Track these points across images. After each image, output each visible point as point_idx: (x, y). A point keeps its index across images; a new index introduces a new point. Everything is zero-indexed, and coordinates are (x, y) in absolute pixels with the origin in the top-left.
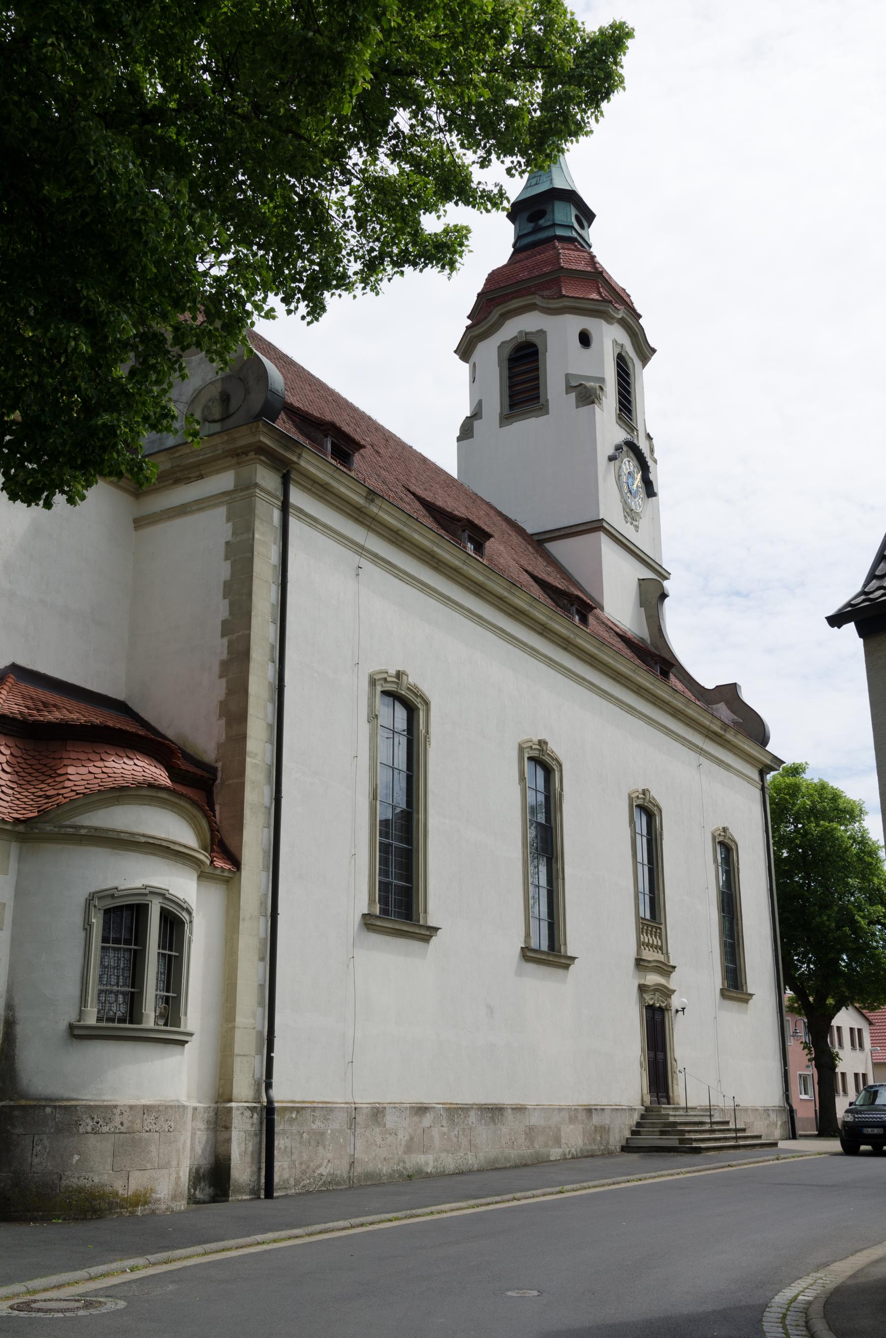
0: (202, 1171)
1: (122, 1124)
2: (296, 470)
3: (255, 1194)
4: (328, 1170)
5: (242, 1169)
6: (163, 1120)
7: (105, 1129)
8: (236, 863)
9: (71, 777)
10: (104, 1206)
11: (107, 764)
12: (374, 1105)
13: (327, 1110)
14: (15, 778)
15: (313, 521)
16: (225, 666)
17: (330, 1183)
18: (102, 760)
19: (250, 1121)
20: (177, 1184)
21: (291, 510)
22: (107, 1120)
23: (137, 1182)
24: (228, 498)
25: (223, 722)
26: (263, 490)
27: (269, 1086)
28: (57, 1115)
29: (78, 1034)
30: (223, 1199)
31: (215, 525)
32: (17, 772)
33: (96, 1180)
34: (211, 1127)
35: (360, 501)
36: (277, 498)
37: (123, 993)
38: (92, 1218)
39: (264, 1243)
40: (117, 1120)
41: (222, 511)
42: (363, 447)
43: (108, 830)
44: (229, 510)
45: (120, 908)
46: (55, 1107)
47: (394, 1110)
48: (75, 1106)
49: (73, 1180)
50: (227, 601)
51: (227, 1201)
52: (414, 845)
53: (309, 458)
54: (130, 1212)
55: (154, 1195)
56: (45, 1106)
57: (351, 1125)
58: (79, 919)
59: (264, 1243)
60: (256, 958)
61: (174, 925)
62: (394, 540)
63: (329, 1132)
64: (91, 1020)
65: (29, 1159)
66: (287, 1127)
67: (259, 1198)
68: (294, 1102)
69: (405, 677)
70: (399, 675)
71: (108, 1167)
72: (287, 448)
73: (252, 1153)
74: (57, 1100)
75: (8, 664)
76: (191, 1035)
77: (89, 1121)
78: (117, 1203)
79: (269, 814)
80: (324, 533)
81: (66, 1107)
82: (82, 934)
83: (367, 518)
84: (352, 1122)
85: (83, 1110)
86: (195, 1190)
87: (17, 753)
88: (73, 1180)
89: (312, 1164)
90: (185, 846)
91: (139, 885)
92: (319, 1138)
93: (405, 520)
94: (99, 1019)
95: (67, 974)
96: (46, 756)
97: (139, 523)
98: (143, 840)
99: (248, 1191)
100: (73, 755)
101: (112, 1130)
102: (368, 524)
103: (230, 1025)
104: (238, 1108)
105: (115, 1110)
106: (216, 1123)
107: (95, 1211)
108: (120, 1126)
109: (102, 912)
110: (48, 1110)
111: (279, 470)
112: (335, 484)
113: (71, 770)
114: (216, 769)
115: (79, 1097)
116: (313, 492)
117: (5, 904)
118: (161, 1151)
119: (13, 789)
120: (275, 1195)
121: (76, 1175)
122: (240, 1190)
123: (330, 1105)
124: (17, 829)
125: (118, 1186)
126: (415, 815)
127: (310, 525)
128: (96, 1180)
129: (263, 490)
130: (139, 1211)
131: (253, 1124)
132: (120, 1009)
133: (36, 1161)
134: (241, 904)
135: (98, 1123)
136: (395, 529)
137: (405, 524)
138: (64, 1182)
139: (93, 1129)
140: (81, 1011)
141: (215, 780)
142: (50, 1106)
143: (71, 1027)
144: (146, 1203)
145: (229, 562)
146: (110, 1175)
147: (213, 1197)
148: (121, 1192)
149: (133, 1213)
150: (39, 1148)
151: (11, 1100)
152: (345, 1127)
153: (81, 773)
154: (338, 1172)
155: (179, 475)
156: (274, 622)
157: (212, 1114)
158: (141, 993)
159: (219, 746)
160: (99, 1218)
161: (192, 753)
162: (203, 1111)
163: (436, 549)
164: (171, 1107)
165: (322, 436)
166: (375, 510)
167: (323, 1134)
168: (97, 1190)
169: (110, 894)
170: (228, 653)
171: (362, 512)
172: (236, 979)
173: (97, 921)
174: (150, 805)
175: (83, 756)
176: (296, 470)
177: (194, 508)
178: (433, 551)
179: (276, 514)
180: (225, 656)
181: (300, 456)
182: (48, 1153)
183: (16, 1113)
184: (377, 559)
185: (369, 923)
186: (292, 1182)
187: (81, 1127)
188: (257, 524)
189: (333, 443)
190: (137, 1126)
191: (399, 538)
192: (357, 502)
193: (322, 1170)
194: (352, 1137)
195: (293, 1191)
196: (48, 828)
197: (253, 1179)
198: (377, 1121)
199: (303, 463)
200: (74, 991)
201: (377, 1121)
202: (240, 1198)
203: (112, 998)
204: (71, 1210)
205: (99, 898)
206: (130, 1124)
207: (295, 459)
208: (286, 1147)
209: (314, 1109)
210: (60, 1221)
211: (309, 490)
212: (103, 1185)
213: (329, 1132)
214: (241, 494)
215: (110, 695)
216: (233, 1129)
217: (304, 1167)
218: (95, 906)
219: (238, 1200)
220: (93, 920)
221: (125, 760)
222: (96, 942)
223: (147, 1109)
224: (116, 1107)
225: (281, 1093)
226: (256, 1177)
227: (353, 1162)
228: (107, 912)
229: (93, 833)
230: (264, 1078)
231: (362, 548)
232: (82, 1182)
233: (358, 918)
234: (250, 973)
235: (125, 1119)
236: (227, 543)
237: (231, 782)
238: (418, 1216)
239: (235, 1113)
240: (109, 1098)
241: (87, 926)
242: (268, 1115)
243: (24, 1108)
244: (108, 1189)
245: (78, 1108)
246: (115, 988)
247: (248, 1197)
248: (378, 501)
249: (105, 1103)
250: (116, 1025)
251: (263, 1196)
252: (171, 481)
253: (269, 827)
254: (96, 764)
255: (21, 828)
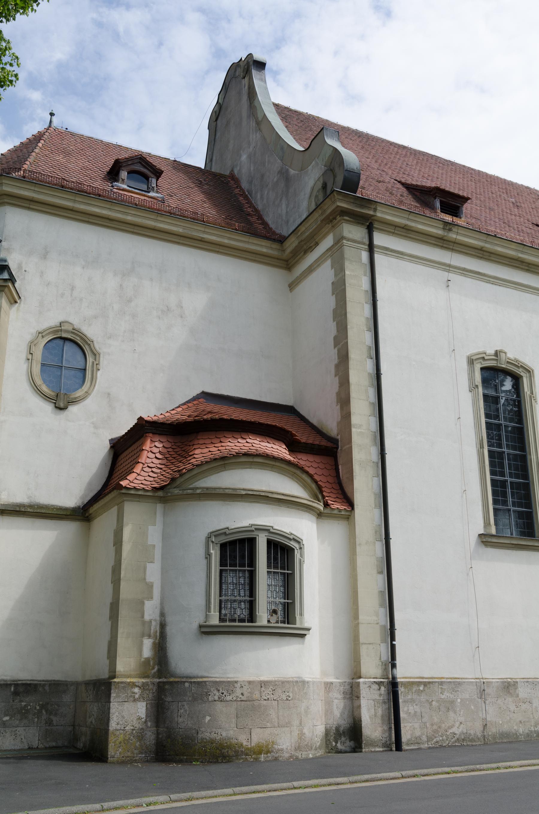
0: (341, 729)
1: (242, 694)
2: (376, 221)
3: (388, 747)
4: (460, 730)
5: (373, 727)
6: (280, 691)
7: (229, 698)
8: (351, 504)
9: (195, 456)
10: (231, 753)
11: (223, 444)
12: (505, 680)
13: (456, 684)
14: (165, 462)
15: (387, 251)
16: (337, 366)
17: (463, 740)
18: (221, 442)
19: (378, 692)
20: (300, 738)
21: (375, 249)
22: (230, 692)
23: (258, 737)
24: (330, 253)
25: (339, 407)
26: (348, 240)
27: (394, 666)
28: (193, 688)
29: (207, 631)
30: (359, 750)
31: (325, 274)
32: (166, 458)
33: (224, 734)
34: (348, 696)
35: (440, 232)
36: (364, 244)
37: (244, 602)
38: (222, 762)
39: (300, 787)
40: (238, 692)
41: (329, 262)
42: (468, 199)
43: (215, 489)
44: (332, 260)
45: (233, 543)
46: (191, 682)
47: (526, 684)
48: (205, 682)
49: (206, 734)
50: (335, 323)
51: (361, 752)
52: (531, 479)
53: (384, 210)
54: (254, 759)
55: (276, 746)
56: (184, 682)
57: (481, 695)
58: (201, 551)
59: (300, 787)
60: (375, 571)
61: (283, 553)
62: (481, 256)
63: (459, 700)
64: (215, 620)
65: (176, 719)
66: (415, 697)
67: (391, 750)
68: (423, 678)
69: (503, 355)
70: (497, 353)
71: (233, 725)
72: (362, 206)
73: (382, 716)
74: (194, 677)
75: (199, 393)
76: (309, 629)
77: (216, 692)
78: (242, 751)
79: (377, 466)
80: (411, 261)
81: (199, 683)
82: (205, 562)
83: (450, 243)
84: (482, 693)
85: (211, 684)
86: (336, 743)
87: (168, 445)
88: (206, 734)
89: (443, 725)
90: (283, 495)
91: (247, 525)
92: (450, 706)
93: (485, 239)
94: (221, 620)
95: (196, 589)
96: (186, 445)
97: (292, 286)
98: (244, 492)
99: (381, 745)
100: (201, 442)
101: (235, 698)
102: (451, 247)
103: (356, 622)
104: (365, 683)
105: (236, 685)
106: (351, 693)
107: (224, 757)
108: (241, 696)
109: (219, 545)
110: (187, 685)
111: (363, 224)
112: (413, 224)
113: (197, 452)
114: (337, 441)
115: (210, 675)
116: (396, 234)
117: (154, 546)
118: (281, 714)
119: (161, 469)
120: (363, 750)
121: (209, 730)
122: (373, 744)
123: (458, 680)
124: (156, 494)
125: (243, 739)
126: (528, 457)
127: (397, 257)
128: (224, 734)
129: (348, 240)
130: (262, 757)
131: (380, 695)
132: (242, 611)
133: (180, 720)
134: (357, 534)
135: (223, 694)
136: (479, 247)
137: (486, 242)
138: (200, 736)
139: (219, 698)
140: (206, 615)
141: (337, 448)
142: (187, 682)
143: (201, 626)
144: (268, 752)
145: (334, 295)
146: (235, 731)
147: (354, 749)
148: (245, 743)
149: (256, 760)
150: (182, 711)
151: (166, 678)
152: (475, 696)
153: (201, 453)
154: (472, 732)
155: (305, 247)
156: (369, 330)
157: (348, 687)
158: (293, 603)
159: (339, 424)
160: (229, 761)
161: (326, 432)
162: (338, 685)
163: (520, 255)
164: (288, 682)
165: (433, 199)
166: (454, 236)
167: (452, 702)
168: (225, 742)
169: (217, 534)
170: (338, 359)
171: (444, 240)
172: (357, 588)
173: (215, 553)
174: (250, 468)
175: (208, 441)
176: (376, 221)
177: (315, 266)
178: (519, 257)
179: (365, 256)
180: (336, 361)
181: (375, 210)
182: (188, 715)
183: (167, 687)
184: (465, 272)
185: (485, 540)
186: (424, 738)
187: (210, 697)
188: (347, 264)
189: (441, 202)
190: (257, 695)
191: (485, 253)
192: (437, 234)
193: (454, 730)
194: (483, 704)
195: (426, 745)
196: (176, 492)
197: (384, 736)
198: (509, 692)
199: (379, 214)
200: (201, 601)
201: (509, 692)
202: (373, 750)
203: (235, 605)
204: (206, 755)
205: (215, 536)
206: (249, 695)
207: (371, 213)
208: (416, 712)
209: (441, 683)
210: (198, 763)
211: (393, 233)
212: (229, 739)
213: (459, 700)
214: (336, 247)
215: (280, 403)
216: (361, 698)
217: (435, 727)
218: (213, 542)
219: (372, 752)
220: (212, 551)
221: (240, 440)
222: (215, 566)
223: (263, 684)
224: (236, 682)
225: (402, 673)
226: (387, 734)
227: (486, 724)
228: (223, 546)
229: (205, 491)
230: (390, 660)
231: (449, 266)
232: (213, 736)
233: (474, 538)
234: (370, 584)
235: (245, 690)
236: (333, 283)
237: (345, 447)
238: (481, 770)
239: (362, 686)
240: (231, 676)
241: (208, 556)
242: (393, 686)
243: (171, 683)
244: (234, 741)
245: (207, 683)
246: (238, 598)
247: (381, 749)
248: (455, 229)
249: (229, 680)
250: (237, 624)
251: (394, 749)
252: (303, 253)
253: (378, 476)
254: (216, 445)
255: (160, 493)
